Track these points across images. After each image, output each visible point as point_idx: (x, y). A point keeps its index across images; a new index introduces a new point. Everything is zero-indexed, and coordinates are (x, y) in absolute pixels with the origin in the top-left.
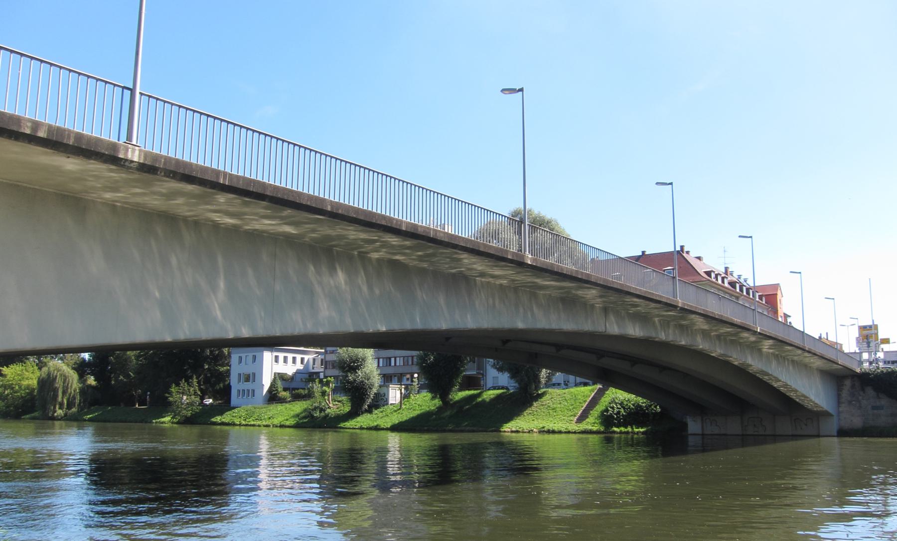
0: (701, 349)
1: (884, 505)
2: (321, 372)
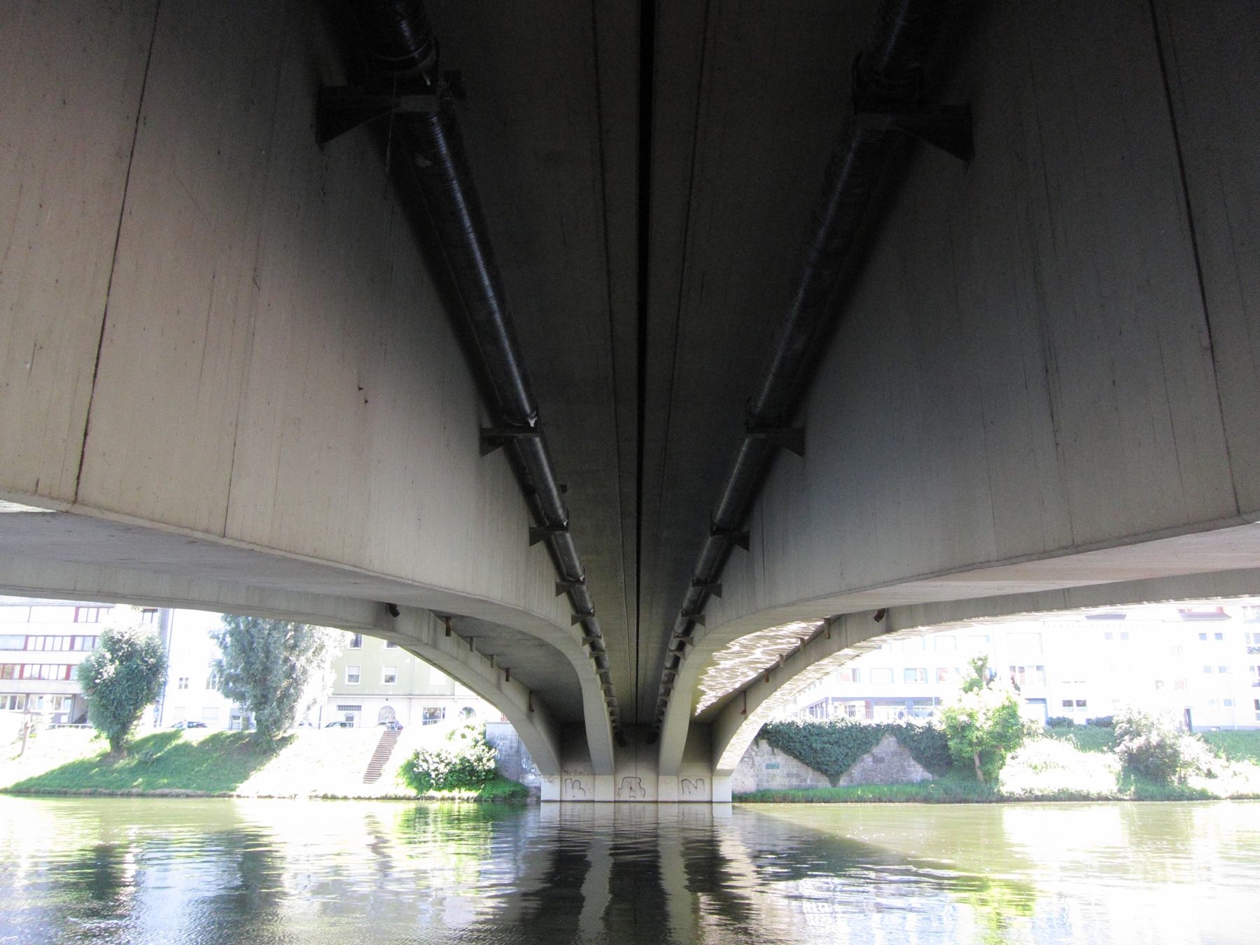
0: (848, 838)
1: (790, 918)
2: (65, 714)
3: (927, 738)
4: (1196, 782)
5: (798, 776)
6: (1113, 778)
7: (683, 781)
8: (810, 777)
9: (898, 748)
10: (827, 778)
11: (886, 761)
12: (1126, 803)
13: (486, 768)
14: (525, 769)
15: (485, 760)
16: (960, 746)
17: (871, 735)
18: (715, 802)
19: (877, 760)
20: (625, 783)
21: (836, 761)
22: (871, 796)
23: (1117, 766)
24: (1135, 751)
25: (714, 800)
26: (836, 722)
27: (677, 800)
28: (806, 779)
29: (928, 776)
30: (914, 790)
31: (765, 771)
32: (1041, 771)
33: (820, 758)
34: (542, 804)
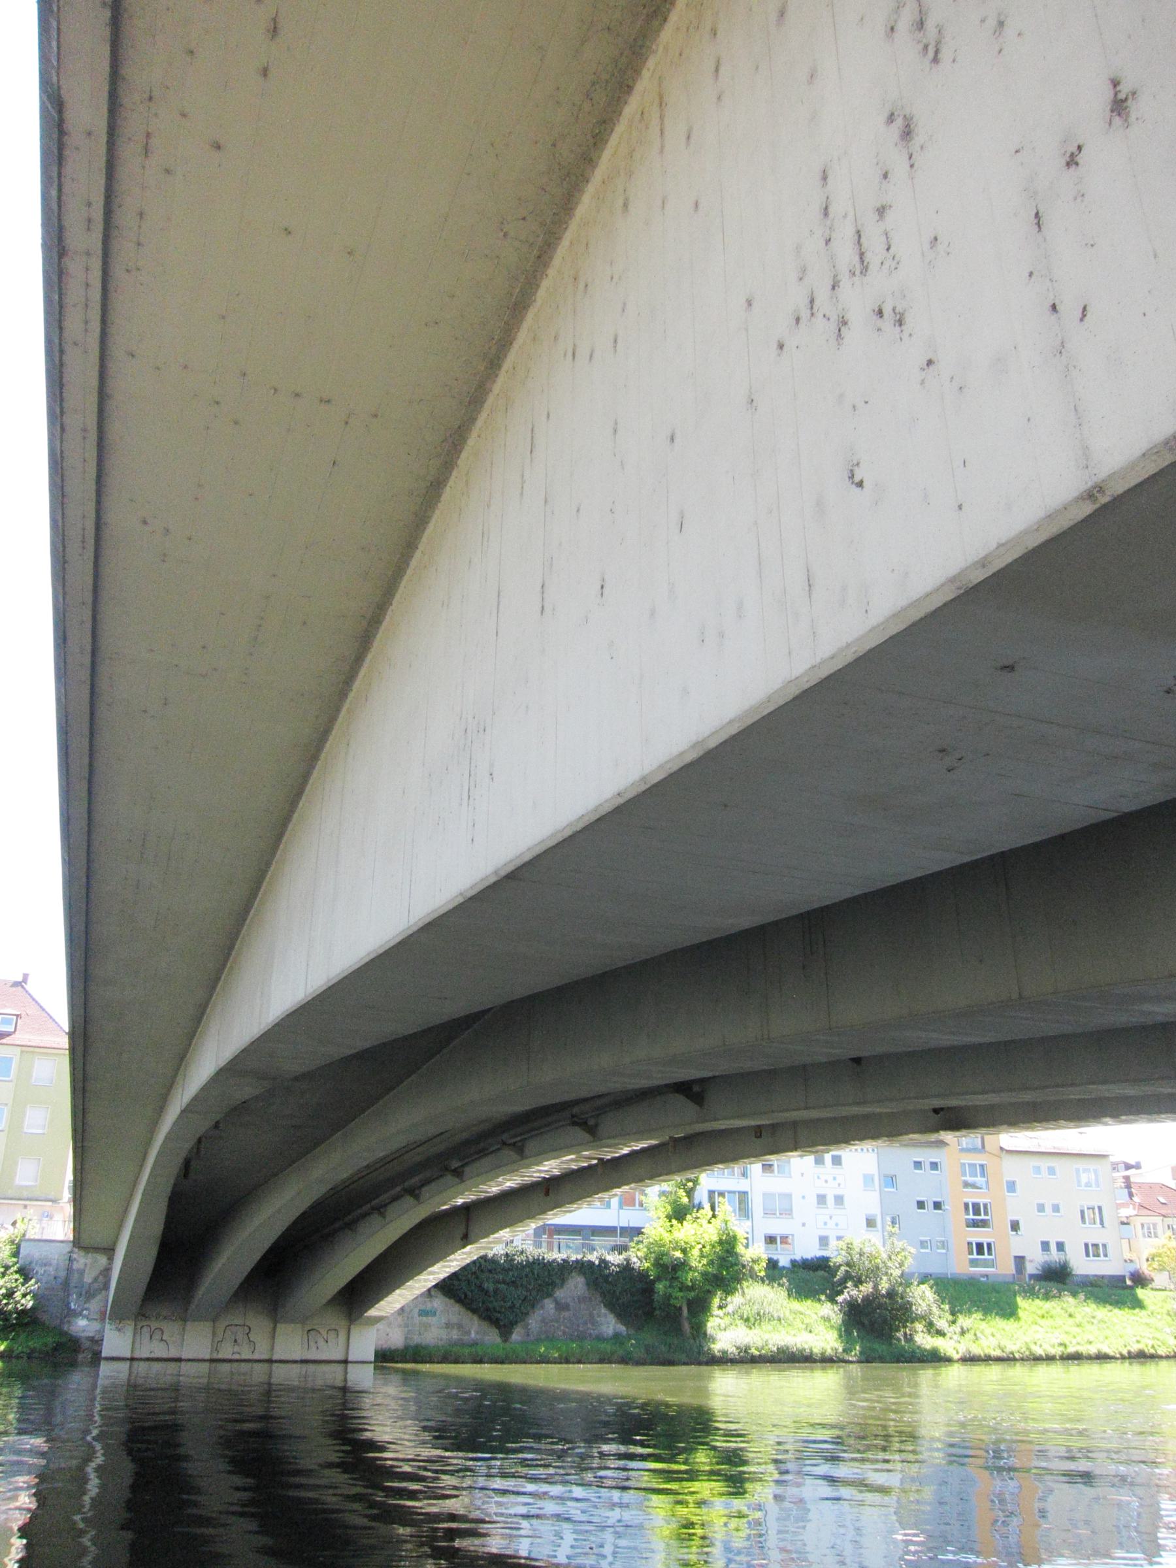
3: (624, 1279)
4: (924, 1340)
5: (460, 1326)
6: (833, 1335)
7: (309, 1331)
8: (476, 1330)
9: (587, 1292)
10: (497, 1331)
11: (571, 1308)
12: (851, 1366)
13: (20, 1308)
14: (74, 1310)
15: (18, 1295)
16: (670, 1290)
17: (556, 1274)
18: (351, 1362)
19: (561, 1307)
20: (228, 1333)
21: (513, 1307)
22: (556, 1355)
23: (837, 1318)
24: (859, 1301)
25: (350, 1359)
26: (514, 1255)
27: (298, 1358)
28: (470, 1332)
29: (622, 1328)
30: (607, 1347)
31: (417, 1319)
32: (754, 1324)
33: (491, 1302)
34: (102, 1363)
